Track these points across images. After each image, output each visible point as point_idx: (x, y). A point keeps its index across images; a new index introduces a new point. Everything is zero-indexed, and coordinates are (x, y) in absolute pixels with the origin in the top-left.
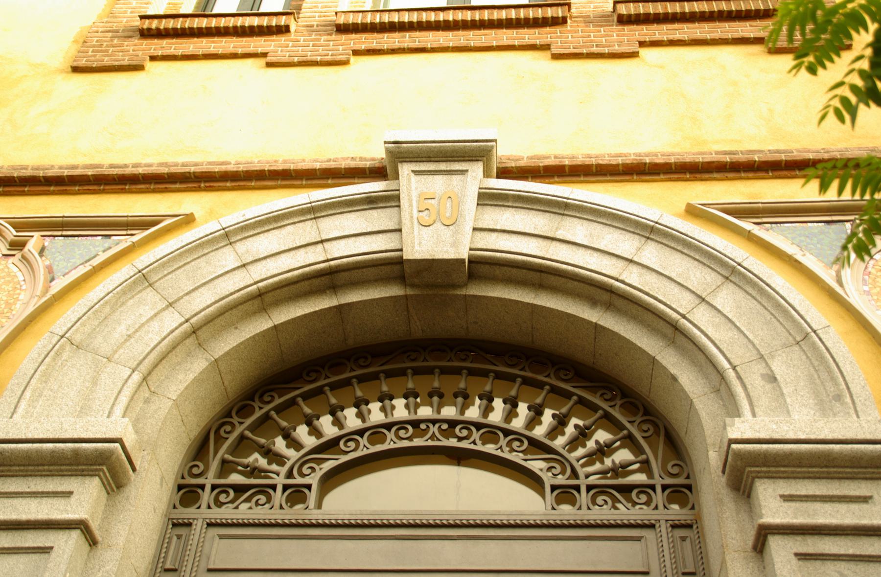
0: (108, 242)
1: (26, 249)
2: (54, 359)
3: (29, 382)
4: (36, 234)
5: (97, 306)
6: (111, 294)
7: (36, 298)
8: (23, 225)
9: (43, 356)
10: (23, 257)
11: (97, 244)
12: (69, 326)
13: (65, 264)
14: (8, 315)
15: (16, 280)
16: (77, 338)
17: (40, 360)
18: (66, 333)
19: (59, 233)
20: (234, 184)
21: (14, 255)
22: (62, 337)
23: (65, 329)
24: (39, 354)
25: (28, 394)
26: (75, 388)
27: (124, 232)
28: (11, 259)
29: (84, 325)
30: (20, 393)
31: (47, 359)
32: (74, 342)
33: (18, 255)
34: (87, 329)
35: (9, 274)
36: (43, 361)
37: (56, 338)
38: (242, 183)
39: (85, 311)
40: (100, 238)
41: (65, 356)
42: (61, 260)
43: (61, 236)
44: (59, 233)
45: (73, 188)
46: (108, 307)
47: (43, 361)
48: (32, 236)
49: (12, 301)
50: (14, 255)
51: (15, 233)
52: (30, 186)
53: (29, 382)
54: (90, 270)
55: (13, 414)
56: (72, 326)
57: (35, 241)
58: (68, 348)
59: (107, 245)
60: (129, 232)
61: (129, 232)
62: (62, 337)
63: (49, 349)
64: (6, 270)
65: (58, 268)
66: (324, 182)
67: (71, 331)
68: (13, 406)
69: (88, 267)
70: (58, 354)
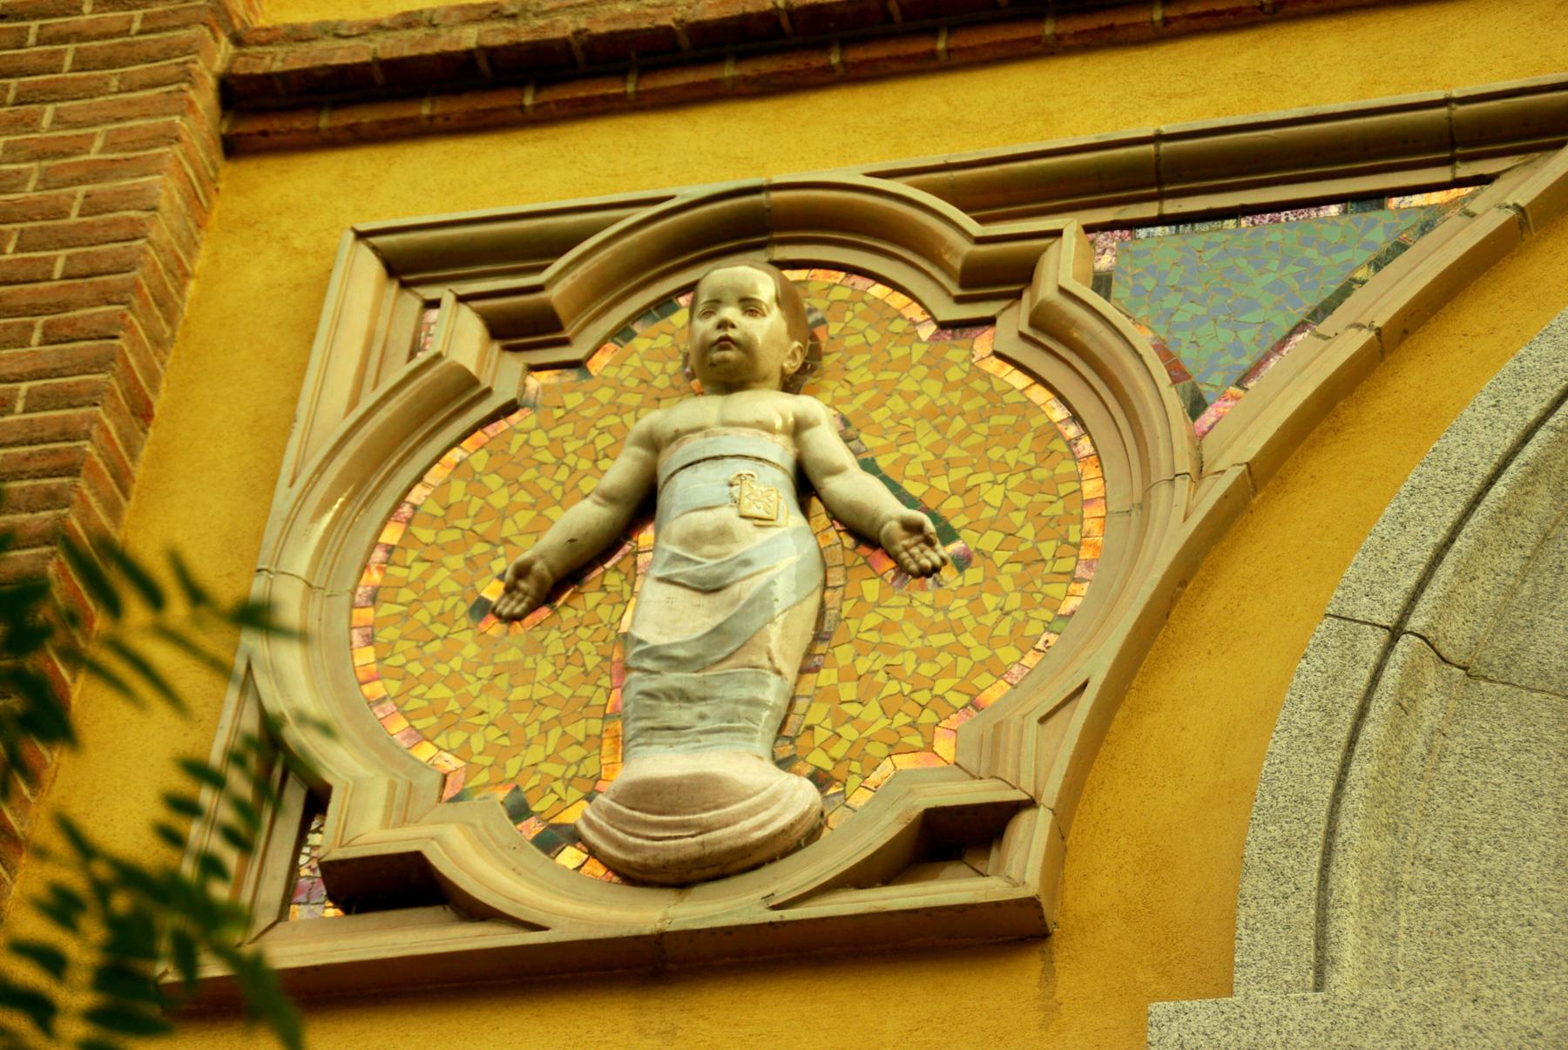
0: (1378, 227)
1: (1045, 289)
2: (1396, 730)
3: (1331, 833)
4: (1070, 224)
5: (1499, 489)
6: (1542, 435)
7: (1183, 486)
8: (1002, 190)
9: (1347, 717)
10: (1048, 328)
11: (1334, 236)
12: (1410, 582)
13: (1226, 336)
14: (1066, 565)
15: (1037, 422)
16: (1457, 634)
17: (1342, 737)
18: (1407, 612)
19: (1150, 210)
20: (749, 69)
21: (990, 321)
22: (1396, 632)
23: (1396, 598)
24: (1329, 715)
25: (1347, 881)
26: (1534, 849)
27: (1443, 174)
28: (983, 343)
29: (1466, 574)
30: (1311, 879)
31: (1370, 731)
32: (1447, 652)
33: (1013, 320)
34: (1483, 591)
35: (991, 394)
36: (1352, 741)
37: (1373, 642)
38: (581, 91)
39: (1452, 515)
40: (1334, 210)
41: (1430, 710)
42: (1197, 321)
43: (1162, 220)
44: (1150, 210)
45: (1140, 17)
46: (1542, 489)
47: (1352, 741)
48: (1058, 234)
49: (1058, 509)
50: (990, 321)
51: (977, 229)
52: (952, 29)
53: (1331, 833)
54: (1368, 345)
55: (1320, 973)
56: (1421, 586)
57: (1068, 257)
58: (1431, 675)
59: (1379, 238)
60: (1465, 171)
61: (1465, 171)
62: (1396, 632)
63: (1362, 685)
64: (978, 384)
65: (1205, 349)
66: (919, 46)
67: (1423, 606)
68: (1307, 937)
69: (1344, 342)
70: (1404, 706)
